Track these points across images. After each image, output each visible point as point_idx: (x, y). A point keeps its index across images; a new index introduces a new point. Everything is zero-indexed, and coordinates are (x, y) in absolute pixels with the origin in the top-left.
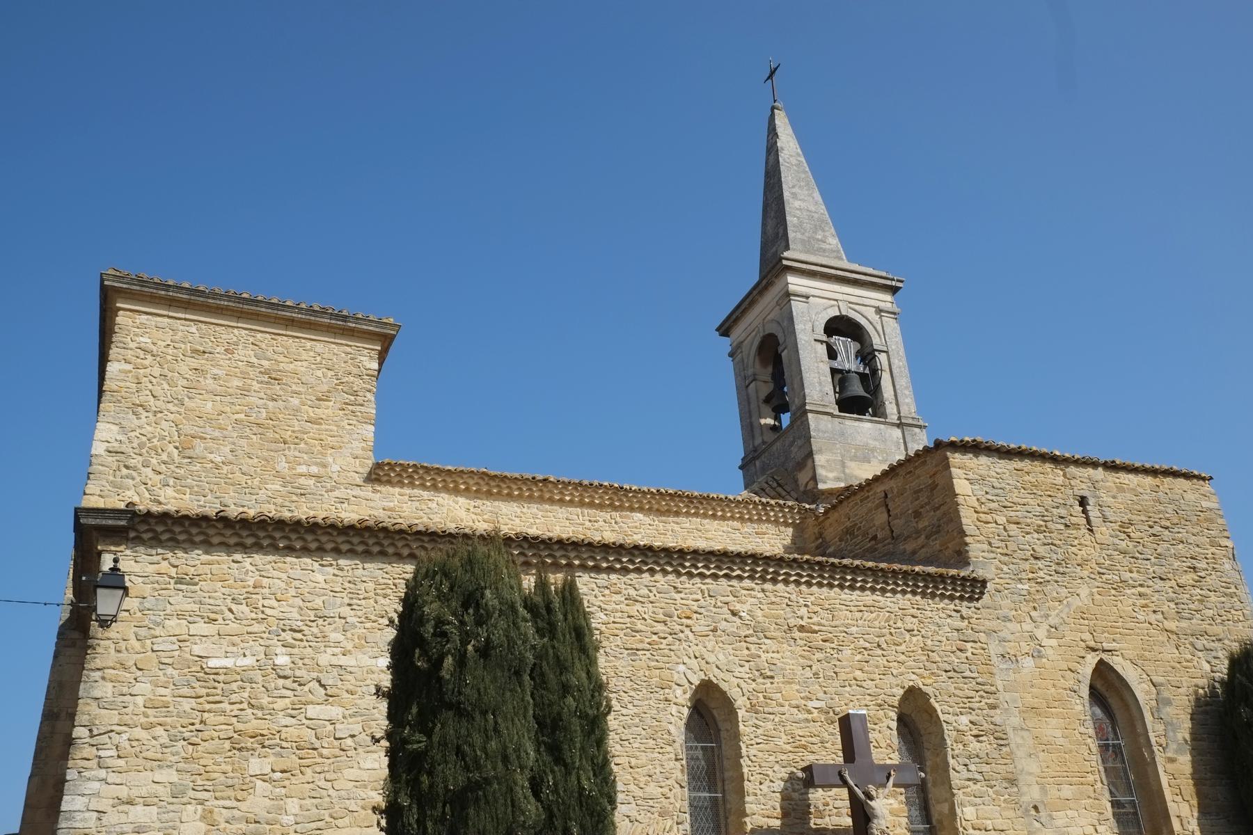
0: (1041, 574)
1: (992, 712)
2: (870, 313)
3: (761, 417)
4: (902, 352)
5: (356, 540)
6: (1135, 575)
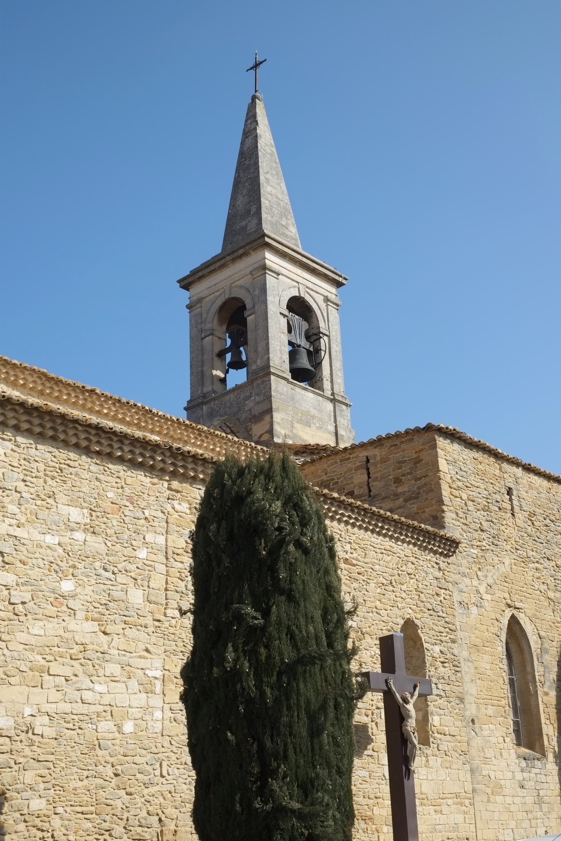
0: (484, 543)
1: (453, 645)
2: (320, 299)
3: (213, 369)
4: (339, 339)
5: (36, 421)
6: (534, 553)
